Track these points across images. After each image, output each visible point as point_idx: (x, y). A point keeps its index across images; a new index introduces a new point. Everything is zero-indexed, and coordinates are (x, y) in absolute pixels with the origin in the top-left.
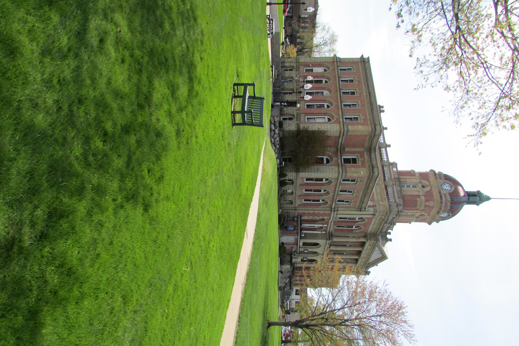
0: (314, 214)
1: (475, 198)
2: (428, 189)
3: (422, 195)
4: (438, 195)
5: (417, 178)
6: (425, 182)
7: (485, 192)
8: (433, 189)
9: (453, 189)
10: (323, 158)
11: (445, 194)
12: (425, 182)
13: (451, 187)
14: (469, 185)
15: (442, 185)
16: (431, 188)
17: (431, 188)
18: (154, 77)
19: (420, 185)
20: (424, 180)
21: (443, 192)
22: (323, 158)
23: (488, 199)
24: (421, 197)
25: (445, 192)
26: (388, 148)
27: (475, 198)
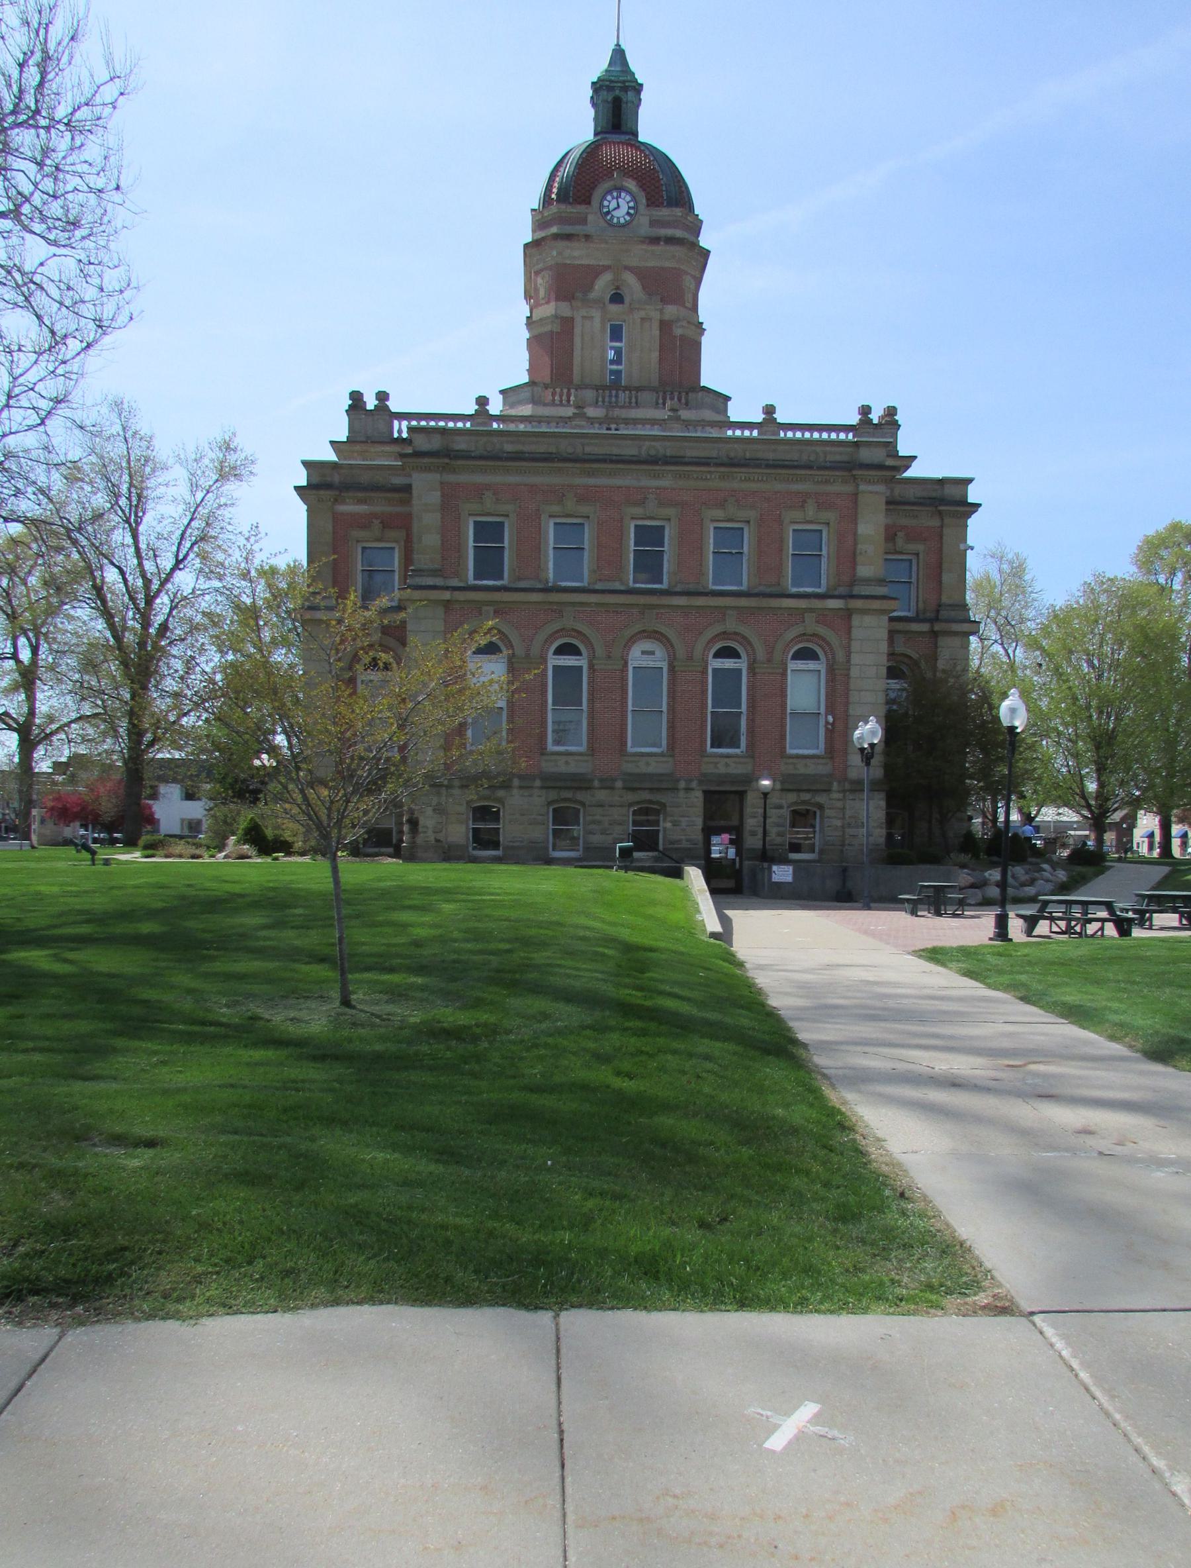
0: (951, 1037)
1: (617, 97)
2: (632, 284)
3: (661, 311)
4: (660, 248)
5: (583, 312)
6: (602, 285)
7: (599, 66)
8: (634, 262)
9: (631, 184)
10: (714, 670)
11: (653, 223)
12: (602, 285)
13: (620, 189)
14: (578, 127)
15: (610, 224)
16: (626, 268)
17: (626, 268)
18: (150, 807)
19: (614, 308)
20: (590, 287)
21: (645, 229)
22: (714, 670)
23: (619, 55)
24: (666, 317)
25: (644, 220)
26: (780, 417)
27: (617, 97)
